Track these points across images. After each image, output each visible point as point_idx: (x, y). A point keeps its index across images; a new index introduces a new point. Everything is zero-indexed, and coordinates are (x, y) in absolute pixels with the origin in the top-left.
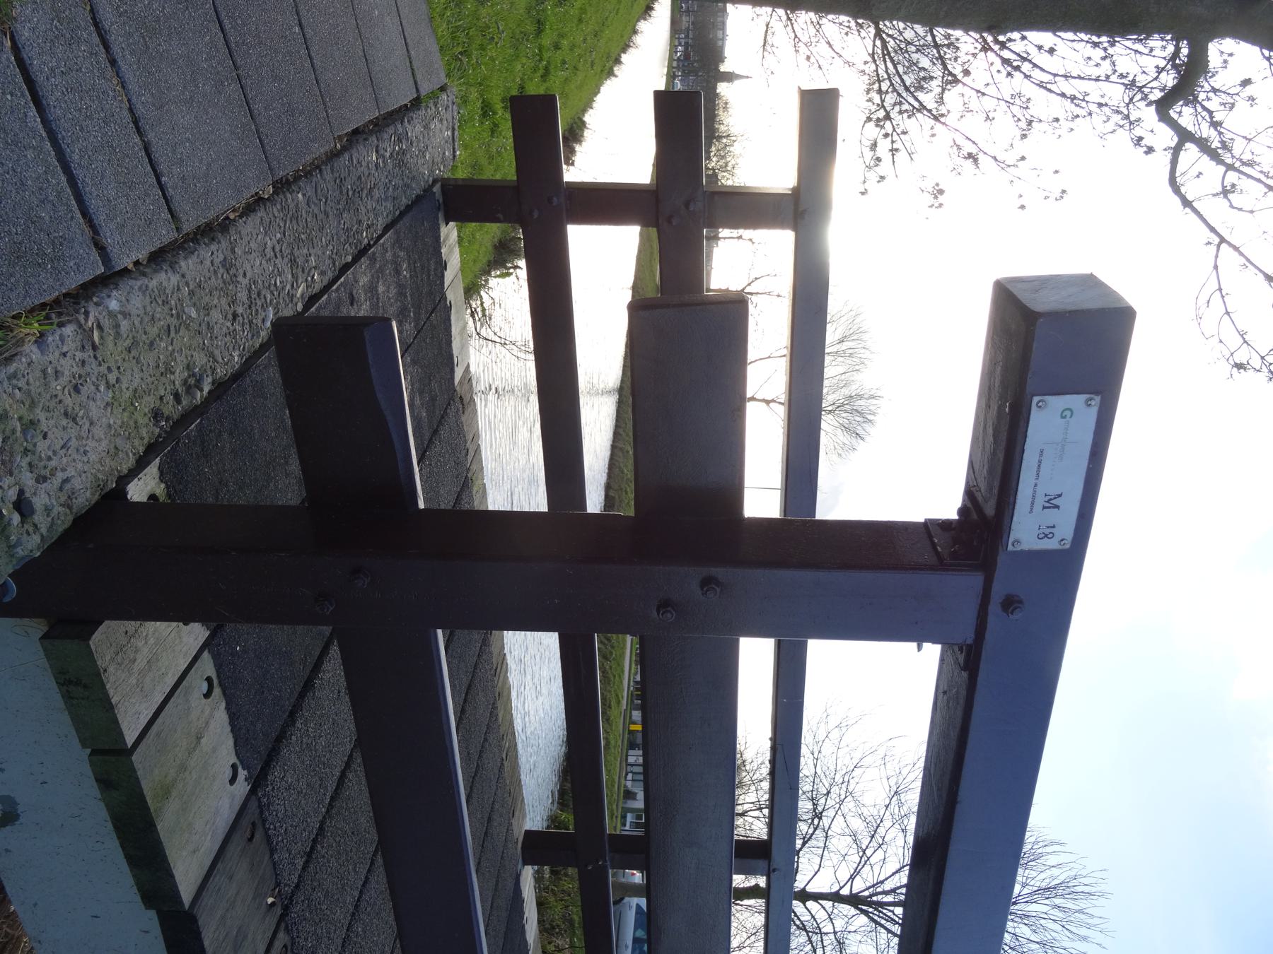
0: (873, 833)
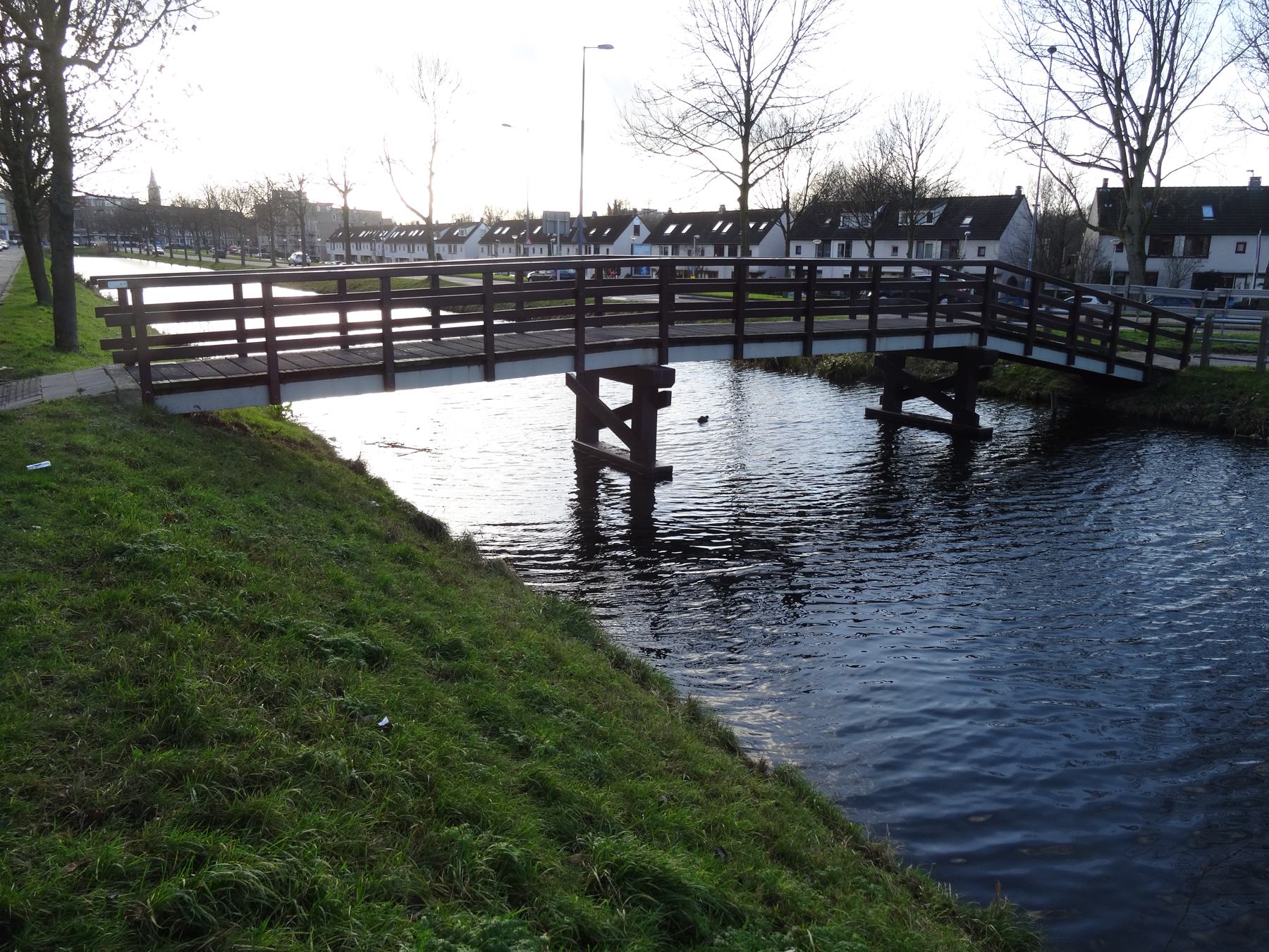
0: (135, 42)
